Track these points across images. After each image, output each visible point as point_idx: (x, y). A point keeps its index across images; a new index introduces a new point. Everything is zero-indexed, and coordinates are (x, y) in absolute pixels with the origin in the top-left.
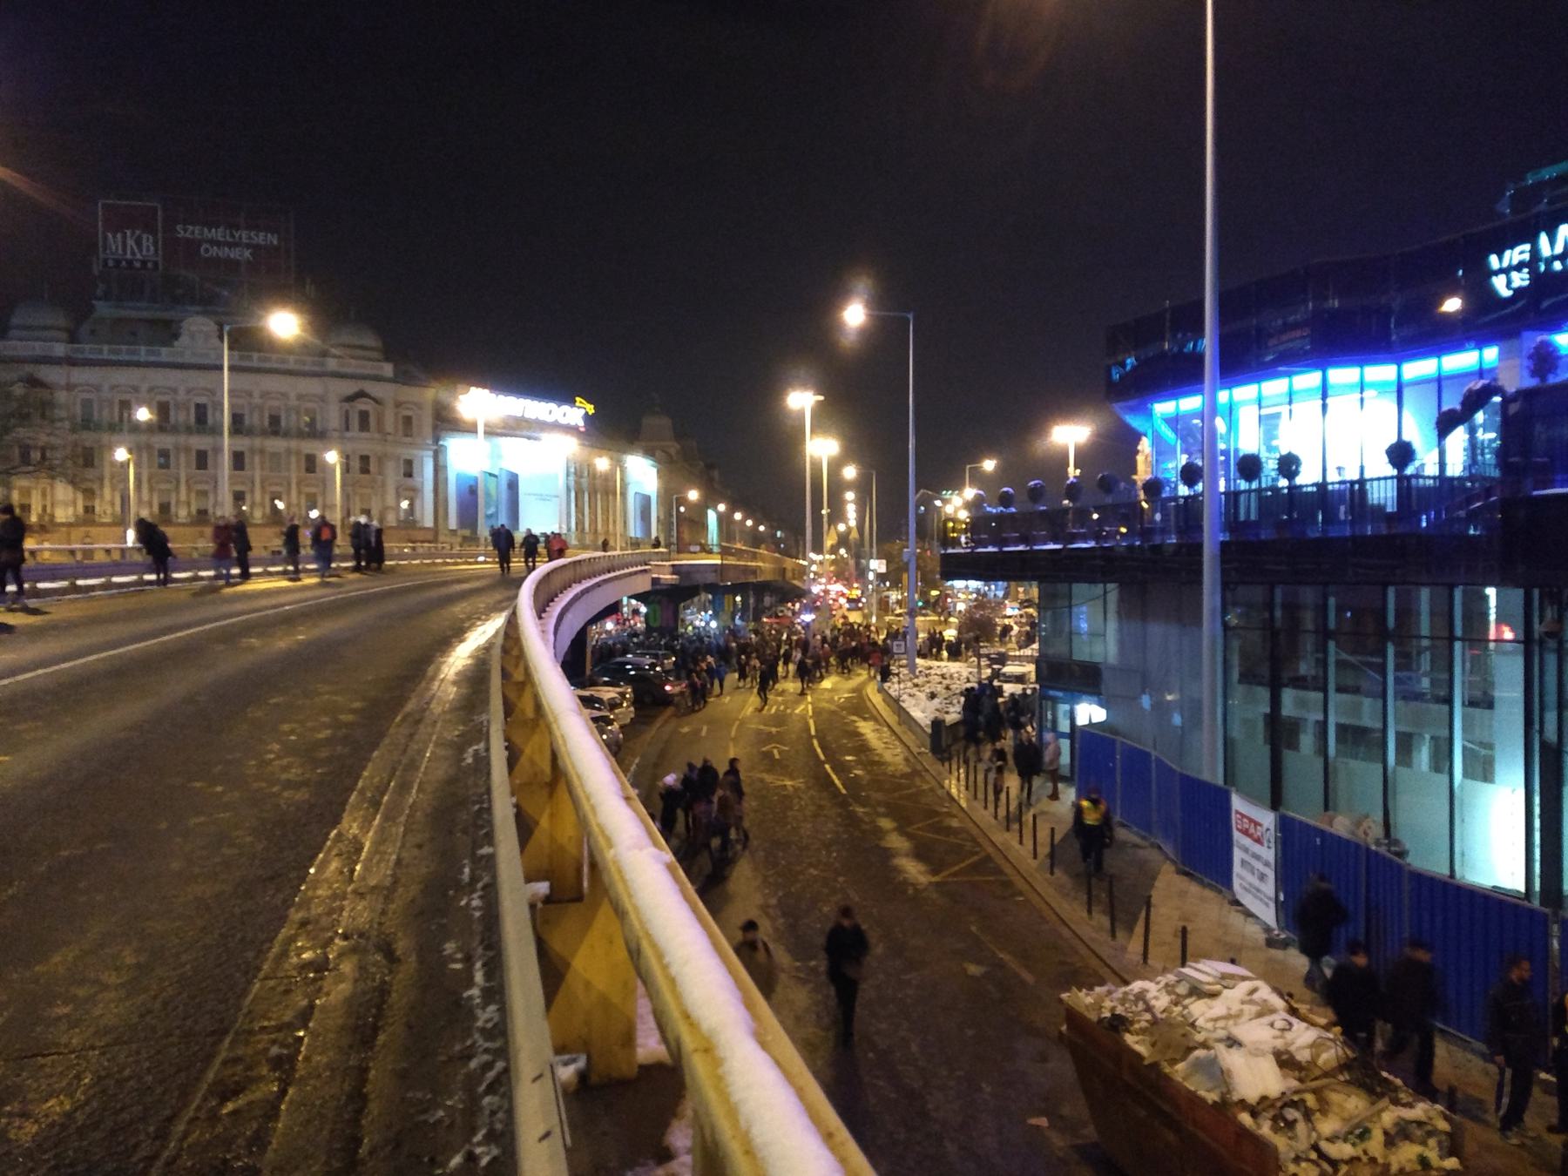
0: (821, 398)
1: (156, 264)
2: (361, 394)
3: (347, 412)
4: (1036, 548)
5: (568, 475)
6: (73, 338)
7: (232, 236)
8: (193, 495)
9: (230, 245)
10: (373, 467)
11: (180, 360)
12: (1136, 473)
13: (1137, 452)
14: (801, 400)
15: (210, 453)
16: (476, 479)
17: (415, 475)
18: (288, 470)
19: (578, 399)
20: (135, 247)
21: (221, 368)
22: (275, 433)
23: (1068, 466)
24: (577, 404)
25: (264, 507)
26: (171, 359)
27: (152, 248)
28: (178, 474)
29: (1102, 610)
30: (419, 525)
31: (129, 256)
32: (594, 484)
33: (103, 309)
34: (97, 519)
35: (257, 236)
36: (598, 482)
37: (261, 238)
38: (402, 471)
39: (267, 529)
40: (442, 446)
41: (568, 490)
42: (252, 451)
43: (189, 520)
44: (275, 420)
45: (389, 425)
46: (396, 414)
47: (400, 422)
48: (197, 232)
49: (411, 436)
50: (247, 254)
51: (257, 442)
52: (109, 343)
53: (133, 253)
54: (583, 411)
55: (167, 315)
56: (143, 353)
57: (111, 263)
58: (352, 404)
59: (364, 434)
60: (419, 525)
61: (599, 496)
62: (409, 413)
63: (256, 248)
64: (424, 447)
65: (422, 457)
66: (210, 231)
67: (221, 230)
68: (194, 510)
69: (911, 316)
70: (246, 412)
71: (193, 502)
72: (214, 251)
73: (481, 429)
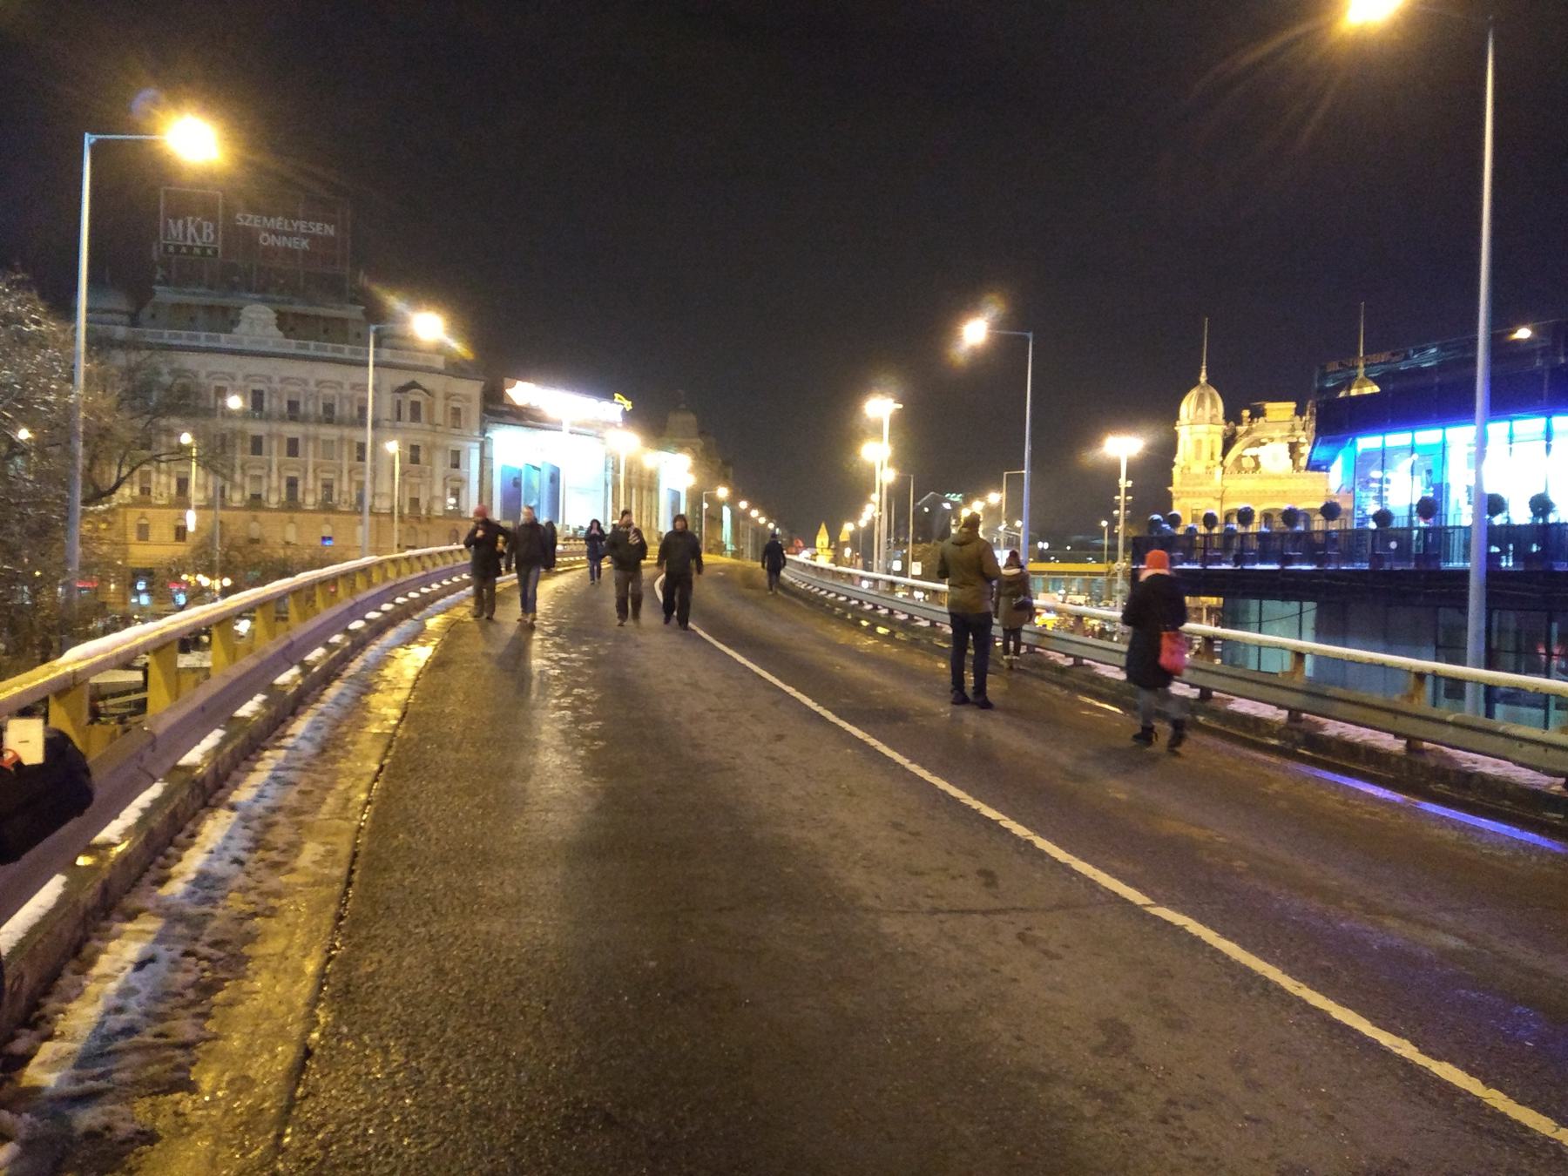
0: (901, 406)
1: (215, 252)
2: (413, 385)
3: (399, 402)
4: (1246, 567)
5: (606, 470)
6: (134, 321)
7: (290, 225)
8: (247, 480)
9: (289, 235)
10: (422, 456)
11: (238, 347)
12: (1171, 485)
13: (1173, 464)
14: (880, 408)
15: (300, 442)
16: (520, 472)
17: (461, 466)
18: (341, 457)
19: (617, 395)
20: (196, 235)
21: (366, 365)
22: (330, 421)
23: (1119, 476)
24: (616, 400)
25: (316, 494)
26: (229, 346)
27: (212, 237)
28: (341, 464)
29: (1298, 628)
30: (464, 515)
31: (189, 243)
32: (630, 480)
33: (164, 295)
34: (153, 500)
35: (315, 226)
36: (645, 479)
37: (317, 228)
38: (450, 462)
39: (282, 514)
40: (488, 438)
41: (606, 485)
42: (307, 438)
43: (243, 504)
44: (329, 408)
45: (439, 418)
46: (446, 406)
47: (449, 412)
48: (256, 221)
49: (459, 428)
50: (305, 243)
51: (312, 429)
52: (171, 327)
53: (193, 240)
54: (621, 407)
55: (227, 301)
56: (203, 338)
57: (171, 249)
58: (404, 394)
59: (414, 425)
60: (464, 515)
61: (634, 491)
62: (456, 405)
63: (313, 238)
64: (471, 439)
65: (469, 448)
66: (269, 219)
67: (280, 218)
68: (248, 494)
69: (1030, 335)
70: (302, 400)
71: (247, 486)
72: (272, 240)
73: (566, 427)
